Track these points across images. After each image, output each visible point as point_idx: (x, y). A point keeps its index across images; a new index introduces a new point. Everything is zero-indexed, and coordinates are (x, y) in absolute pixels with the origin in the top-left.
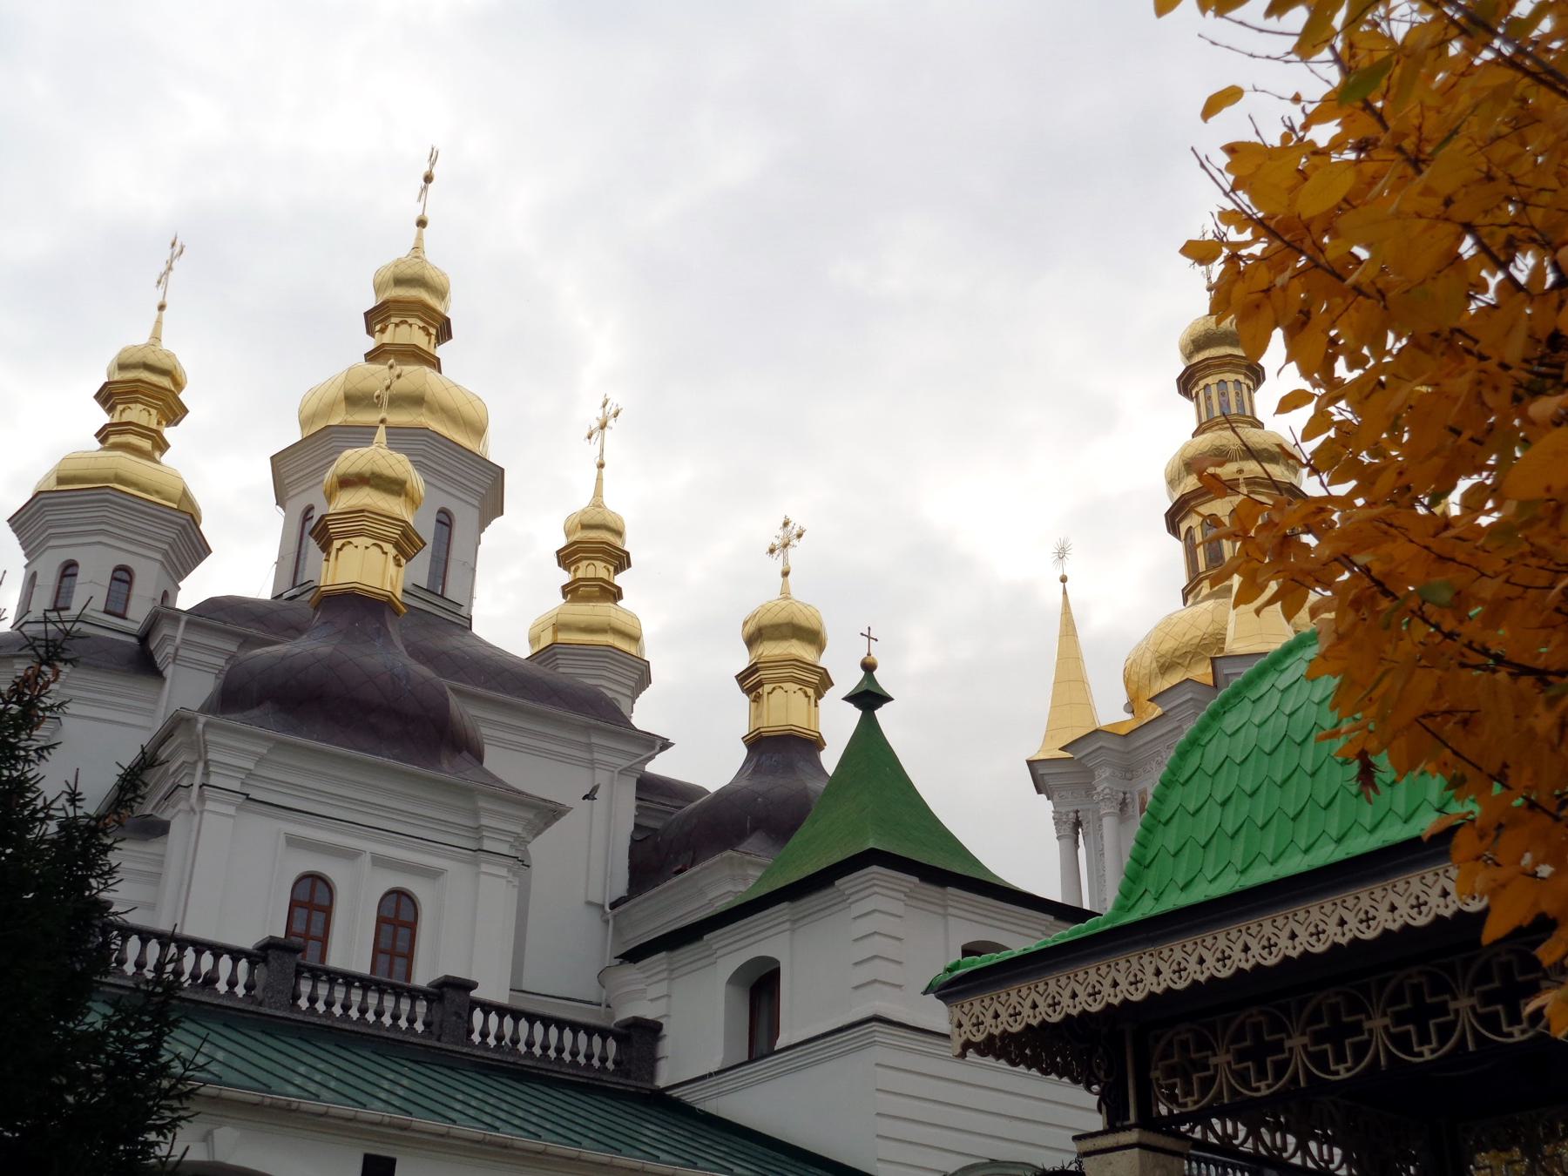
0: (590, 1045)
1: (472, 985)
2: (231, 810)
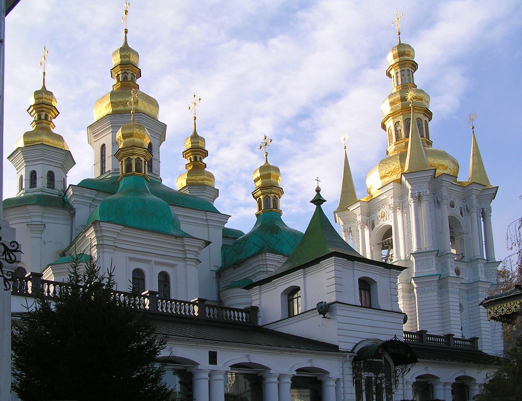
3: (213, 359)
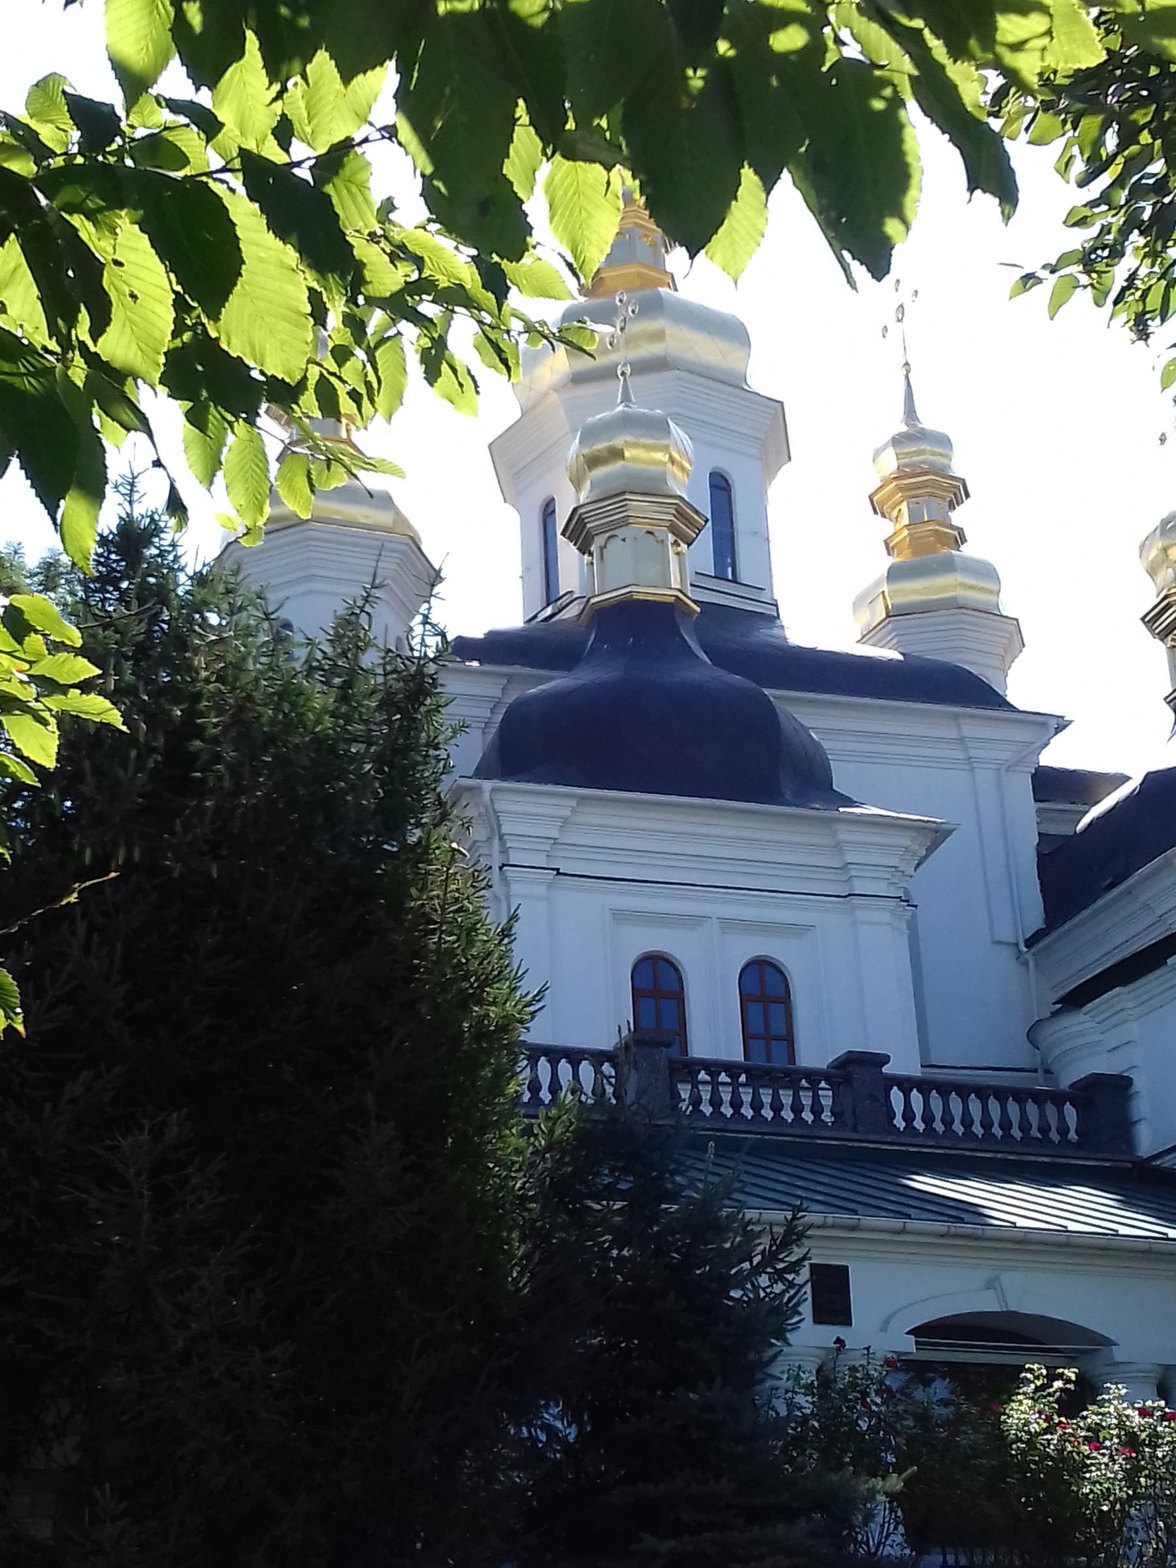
0: (1042, 1115)
1: (884, 1059)
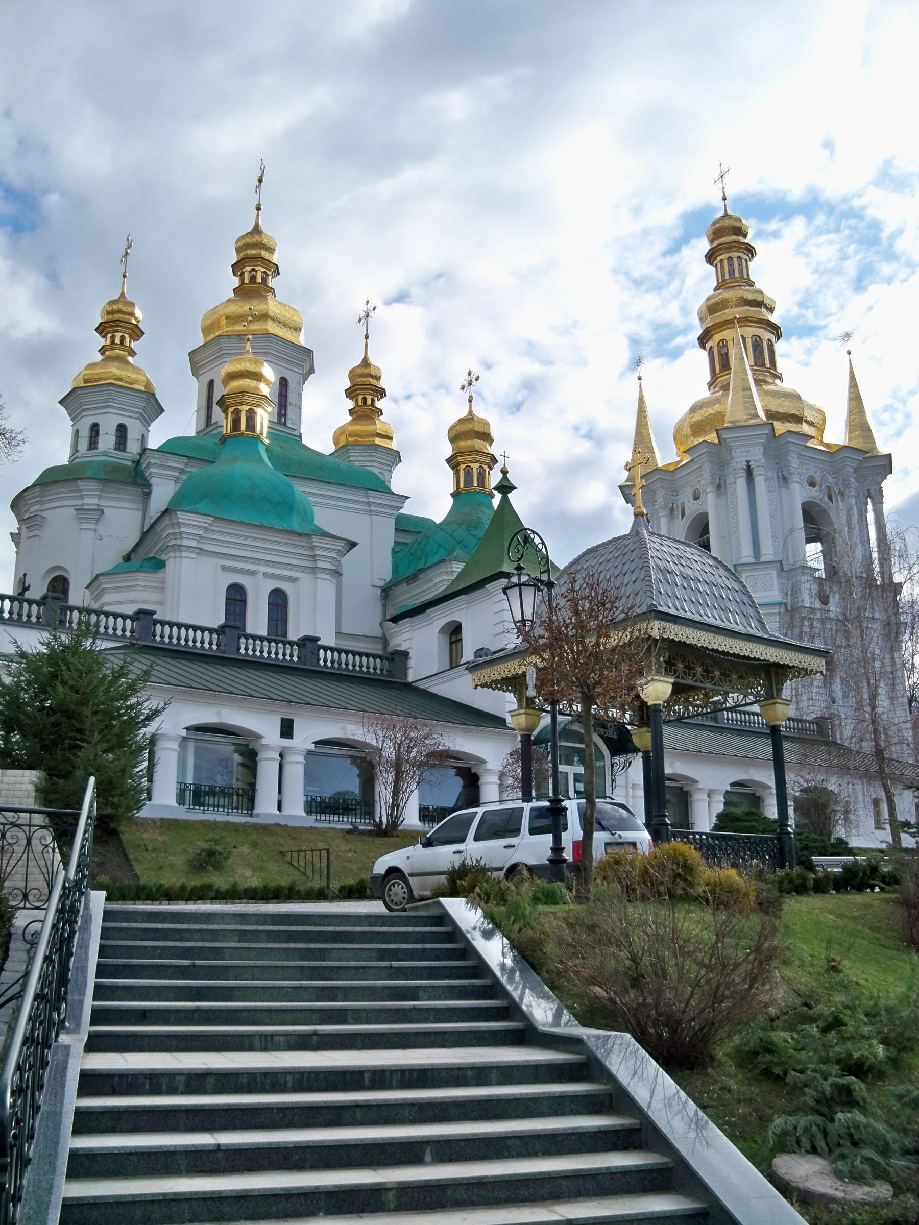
2: (194, 556)
3: (287, 730)
